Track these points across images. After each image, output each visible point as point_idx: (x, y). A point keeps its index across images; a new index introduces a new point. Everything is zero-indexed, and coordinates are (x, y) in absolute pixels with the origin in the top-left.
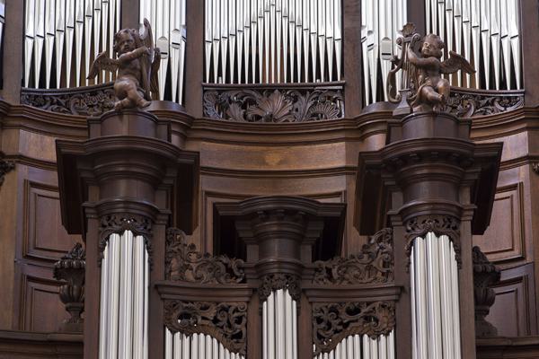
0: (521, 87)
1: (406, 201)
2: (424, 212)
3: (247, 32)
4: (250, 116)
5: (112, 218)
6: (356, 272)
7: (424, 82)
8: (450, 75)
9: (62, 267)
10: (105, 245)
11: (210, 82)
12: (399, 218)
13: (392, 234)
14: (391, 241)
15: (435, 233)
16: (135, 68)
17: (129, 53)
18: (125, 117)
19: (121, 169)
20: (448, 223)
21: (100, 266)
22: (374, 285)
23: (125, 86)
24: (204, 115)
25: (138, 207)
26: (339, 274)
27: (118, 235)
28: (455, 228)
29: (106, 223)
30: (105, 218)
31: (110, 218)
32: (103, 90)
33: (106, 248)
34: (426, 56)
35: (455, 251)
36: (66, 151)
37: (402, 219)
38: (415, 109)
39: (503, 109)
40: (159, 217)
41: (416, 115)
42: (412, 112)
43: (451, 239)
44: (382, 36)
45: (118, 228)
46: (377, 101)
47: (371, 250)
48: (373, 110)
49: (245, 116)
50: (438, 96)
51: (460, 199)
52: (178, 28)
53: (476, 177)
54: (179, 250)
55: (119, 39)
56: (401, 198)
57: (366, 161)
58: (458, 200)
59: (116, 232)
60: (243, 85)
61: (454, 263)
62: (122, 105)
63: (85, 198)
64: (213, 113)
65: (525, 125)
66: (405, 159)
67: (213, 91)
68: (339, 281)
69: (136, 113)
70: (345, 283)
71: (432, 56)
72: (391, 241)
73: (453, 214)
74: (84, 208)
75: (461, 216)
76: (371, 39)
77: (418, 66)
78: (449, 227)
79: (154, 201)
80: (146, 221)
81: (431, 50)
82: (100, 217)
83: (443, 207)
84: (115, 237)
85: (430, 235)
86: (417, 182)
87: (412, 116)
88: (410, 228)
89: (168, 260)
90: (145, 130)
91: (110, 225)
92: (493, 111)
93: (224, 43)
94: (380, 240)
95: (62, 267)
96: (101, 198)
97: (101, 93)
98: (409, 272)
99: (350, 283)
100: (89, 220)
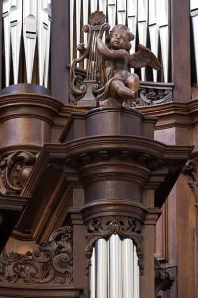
0: (170, 80)
1: (87, 200)
2: (109, 212)
6: (32, 270)
7: (113, 76)
8: (143, 70)
12: (80, 217)
13: (72, 233)
14: (71, 240)
15: (119, 236)
19: (109, 170)
20: (133, 226)
22: (51, 285)
26: (15, 272)
28: (139, 232)
34: (116, 48)
35: (139, 256)
36: (55, 154)
37: (84, 219)
38: (102, 103)
39: (149, 101)
41: (103, 110)
42: (98, 105)
43: (135, 243)
44: (26, 14)
45: (103, 233)
46: (19, 82)
47: (48, 248)
48: (14, 92)
50: (131, 92)
51: (144, 200)
53: (162, 180)
56: (83, 196)
58: (142, 202)
61: (137, 269)
65: (172, 121)
66: (94, 155)
68: (15, 279)
70: (21, 281)
71: (121, 48)
72: (71, 240)
73: (138, 217)
75: (145, 219)
76: (15, 15)
77: (106, 58)
78: (133, 230)
81: (122, 41)
83: (129, 209)
84: (101, 242)
85: (114, 238)
86: (102, 180)
87: (100, 110)
88: (93, 229)
91: (96, 230)
92: (138, 103)
94: (58, 239)
98: (88, 275)
99: (26, 281)
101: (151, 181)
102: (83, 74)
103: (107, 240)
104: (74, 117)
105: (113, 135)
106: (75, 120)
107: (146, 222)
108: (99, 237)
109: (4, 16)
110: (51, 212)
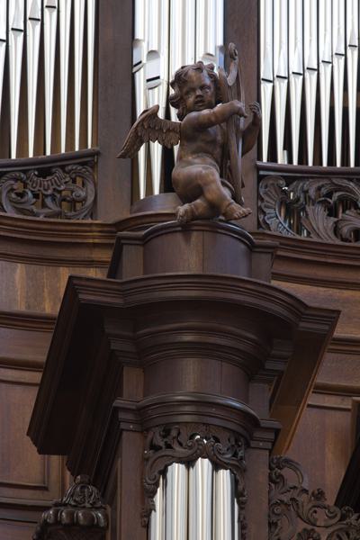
3: (339, 64)
4: (345, 230)
5: (174, 433)
9: (57, 522)
10: (157, 485)
11: (342, 164)
16: (214, 142)
17: (206, 112)
18: (195, 236)
19: (188, 338)
21: (147, 526)
23: (200, 176)
24: (259, 225)
25: (222, 413)
27: (182, 467)
29: (160, 442)
30: (158, 431)
31: (167, 433)
32: (63, 167)
33: (159, 490)
40: (257, 434)
49: (336, 230)
52: (212, 52)
54: (293, 499)
55: (185, 82)
57: (81, 296)
59: (180, 461)
60: (331, 168)
62: (192, 211)
63: (118, 392)
64: (278, 223)
67: (277, 178)
69: (215, 229)
74: (117, 409)
79: (246, 400)
80: (236, 441)
82: (148, 430)
84: (177, 470)
85: (203, 465)
89: (274, 519)
90: (232, 261)
91: (169, 446)
93: (296, 83)
95: (57, 522)
96: (146, 393)
97: (59, 173)
100: (125, 434)
101: (267, 367)
102: (59, 164)
103: (188, 468)
104: (123, 241)
105: (197, 273)
106: (125, 247)
107: (253, 444)
108: (174, 459)
109: (135, 69)
110: (133, 410)
